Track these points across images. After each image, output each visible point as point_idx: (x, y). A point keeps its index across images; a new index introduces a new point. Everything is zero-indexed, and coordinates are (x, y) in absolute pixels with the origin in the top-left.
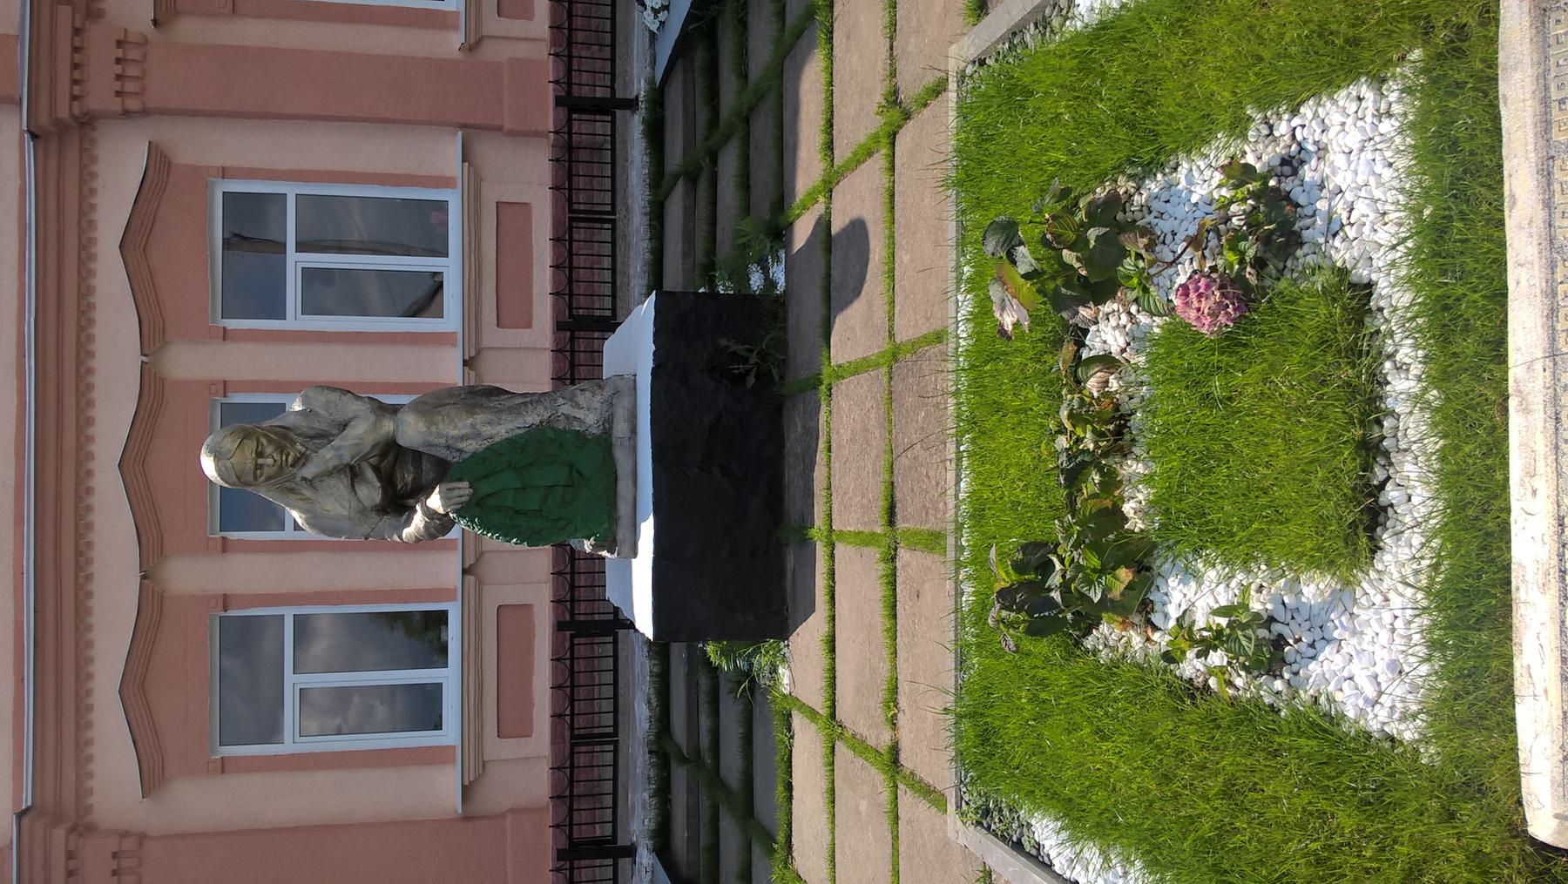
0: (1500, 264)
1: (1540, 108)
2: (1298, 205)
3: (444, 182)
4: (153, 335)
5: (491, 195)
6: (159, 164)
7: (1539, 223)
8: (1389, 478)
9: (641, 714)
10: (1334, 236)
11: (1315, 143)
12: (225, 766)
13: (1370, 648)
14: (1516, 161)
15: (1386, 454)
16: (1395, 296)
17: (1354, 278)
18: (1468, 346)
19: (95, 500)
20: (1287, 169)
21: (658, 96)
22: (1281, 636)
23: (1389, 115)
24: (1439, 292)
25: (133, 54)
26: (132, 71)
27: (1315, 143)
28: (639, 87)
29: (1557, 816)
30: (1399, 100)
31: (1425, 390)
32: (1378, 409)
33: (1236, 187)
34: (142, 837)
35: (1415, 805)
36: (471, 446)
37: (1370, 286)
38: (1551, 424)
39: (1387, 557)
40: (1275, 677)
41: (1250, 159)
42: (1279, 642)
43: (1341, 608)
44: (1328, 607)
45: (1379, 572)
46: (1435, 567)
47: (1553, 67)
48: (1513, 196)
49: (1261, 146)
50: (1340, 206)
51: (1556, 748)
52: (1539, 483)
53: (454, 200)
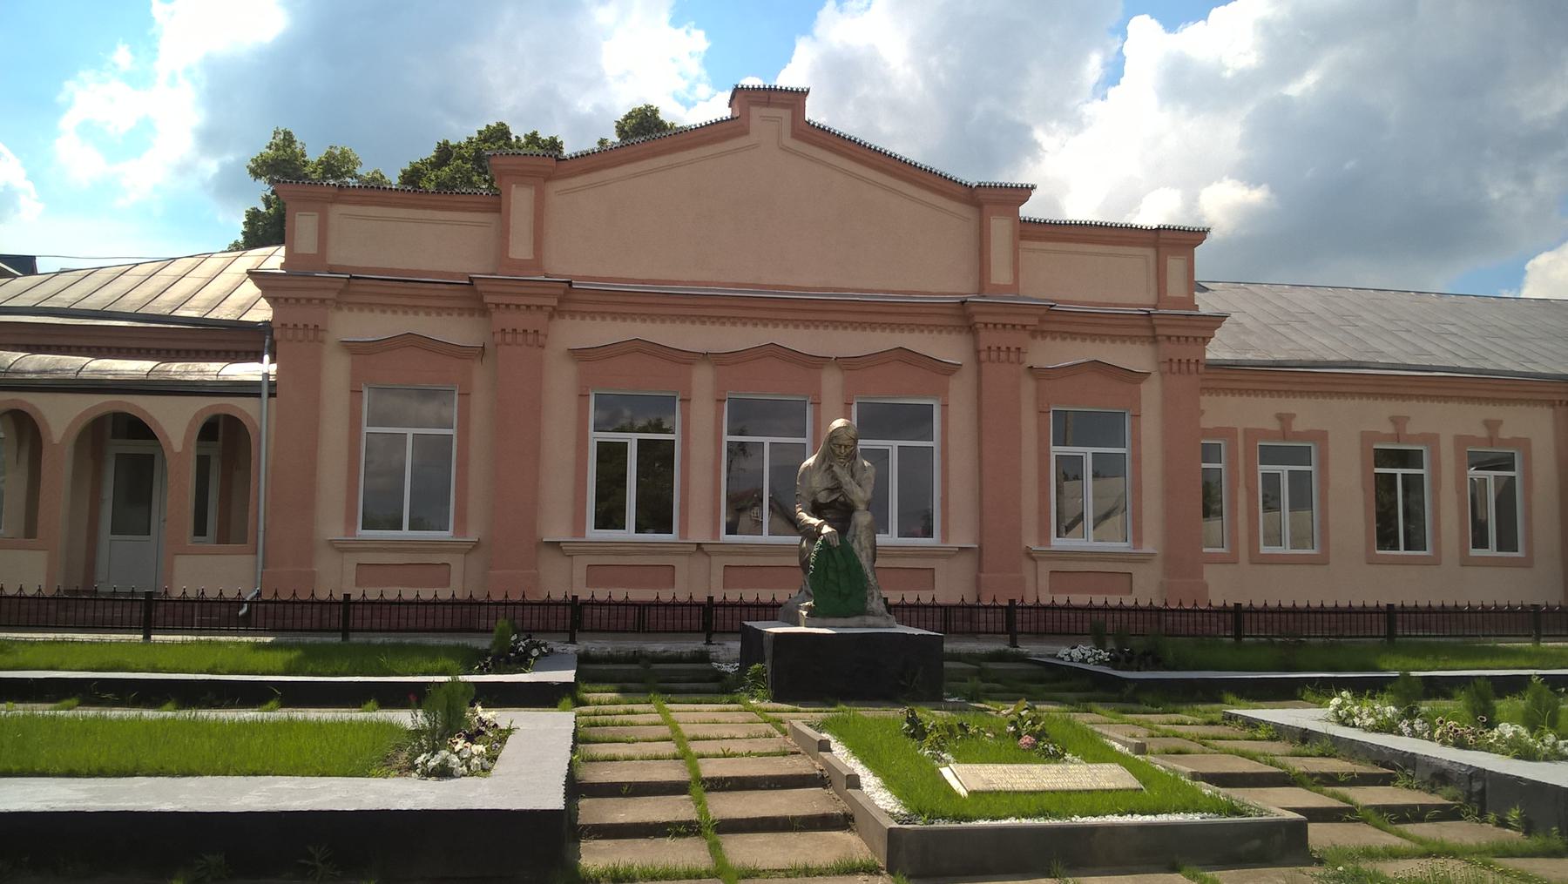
3: (945, 535)
4: (846, 364)
5: (939, 565)
6: (950, 370)
9: (657, 647)
12: (584, 396)
19: (749, 328)
21: (1022, 658)
25: (1013, 356)
26: (1003, 356)
28: (1024, 648)
34: (542, 347)
36: (856, 546)
53: (933, 541)
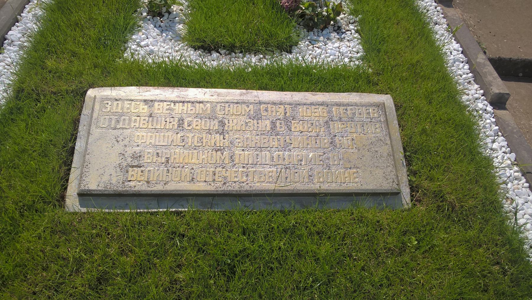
0: (294, 90)
1: (345, 103)
2: (322, 30)
7: (305, 101)
8: (221, 54)
10: (310, 42)
11: (344, 38)
13: (159, 45)
14: (328, 96)
15: (230, 54)
16: (286, 59)
17: (293, 47)
18: (266, 80)
20: (336, 28)
22: (163, 16)
23: (350, 61)
24: (285, 72)
27: (344, 38)
29: (95, 96)
30: (355, 64)
31: (251, 67)
32: (246, 52)
33: (333, 8)
35: (99, 54)
37: (290, 52)
38: (235, 101)
39: (192, 52)
40: (148, 13)
41: (342, 16)
42: (161, 15)
43: (173, 36)
44: (174, 32)
45: (187, 49)
46: (187, 66)
47: (359, 108)
48: (316, 95)
49: (346, 20)
50: (321, 44)
51: (120, 97)
52: (215, 97)
